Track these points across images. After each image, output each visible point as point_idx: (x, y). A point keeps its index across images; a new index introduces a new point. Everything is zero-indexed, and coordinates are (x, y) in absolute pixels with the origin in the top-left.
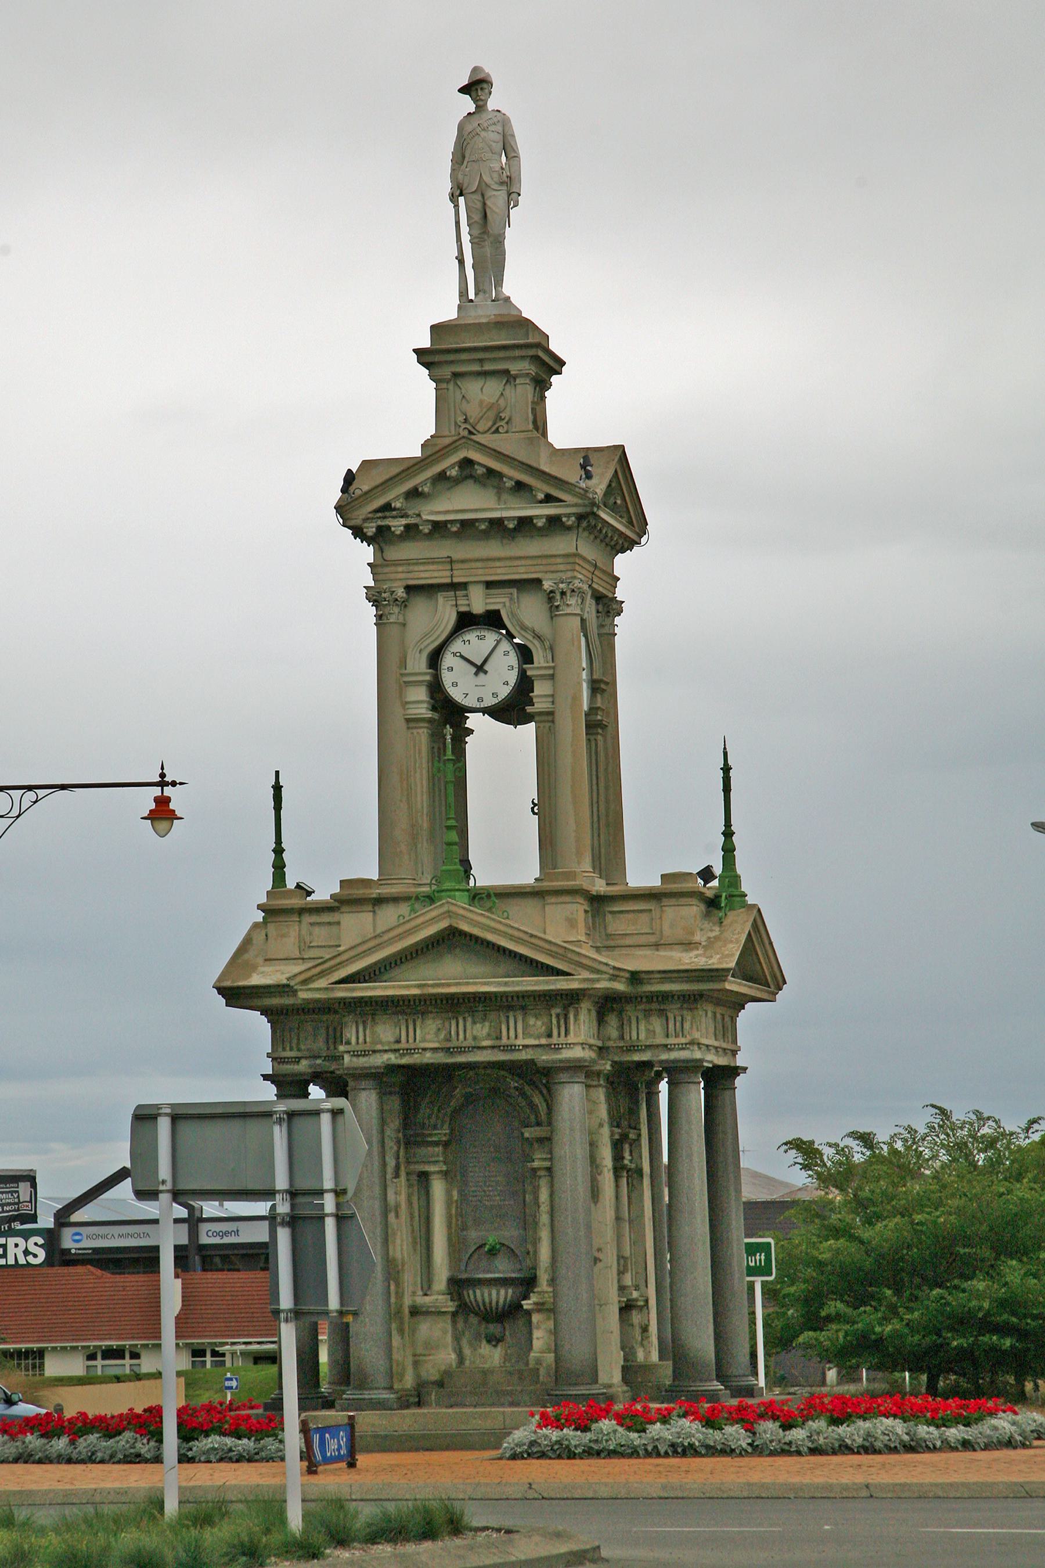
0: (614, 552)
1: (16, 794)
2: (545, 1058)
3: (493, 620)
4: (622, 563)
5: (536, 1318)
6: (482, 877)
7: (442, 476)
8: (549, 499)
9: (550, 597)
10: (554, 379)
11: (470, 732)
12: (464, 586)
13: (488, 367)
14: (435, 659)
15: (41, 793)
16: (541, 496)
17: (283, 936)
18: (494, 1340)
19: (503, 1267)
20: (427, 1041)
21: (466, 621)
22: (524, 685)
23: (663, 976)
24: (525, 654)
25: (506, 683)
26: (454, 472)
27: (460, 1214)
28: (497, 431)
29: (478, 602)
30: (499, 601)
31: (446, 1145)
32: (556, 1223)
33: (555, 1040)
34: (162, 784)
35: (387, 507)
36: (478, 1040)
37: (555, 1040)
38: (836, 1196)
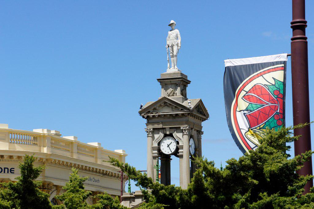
3: (171, 135)
4: (203, 124)
8: (182, 110)
10: (188, 85)
11: (172, 159)
16: (180, 109)
17: (126, 203)
21: (166, 136)
22: (177, 149)
24: (178, 143)
25: (174, 149)
28: (174, 96)
38: (307, 198)
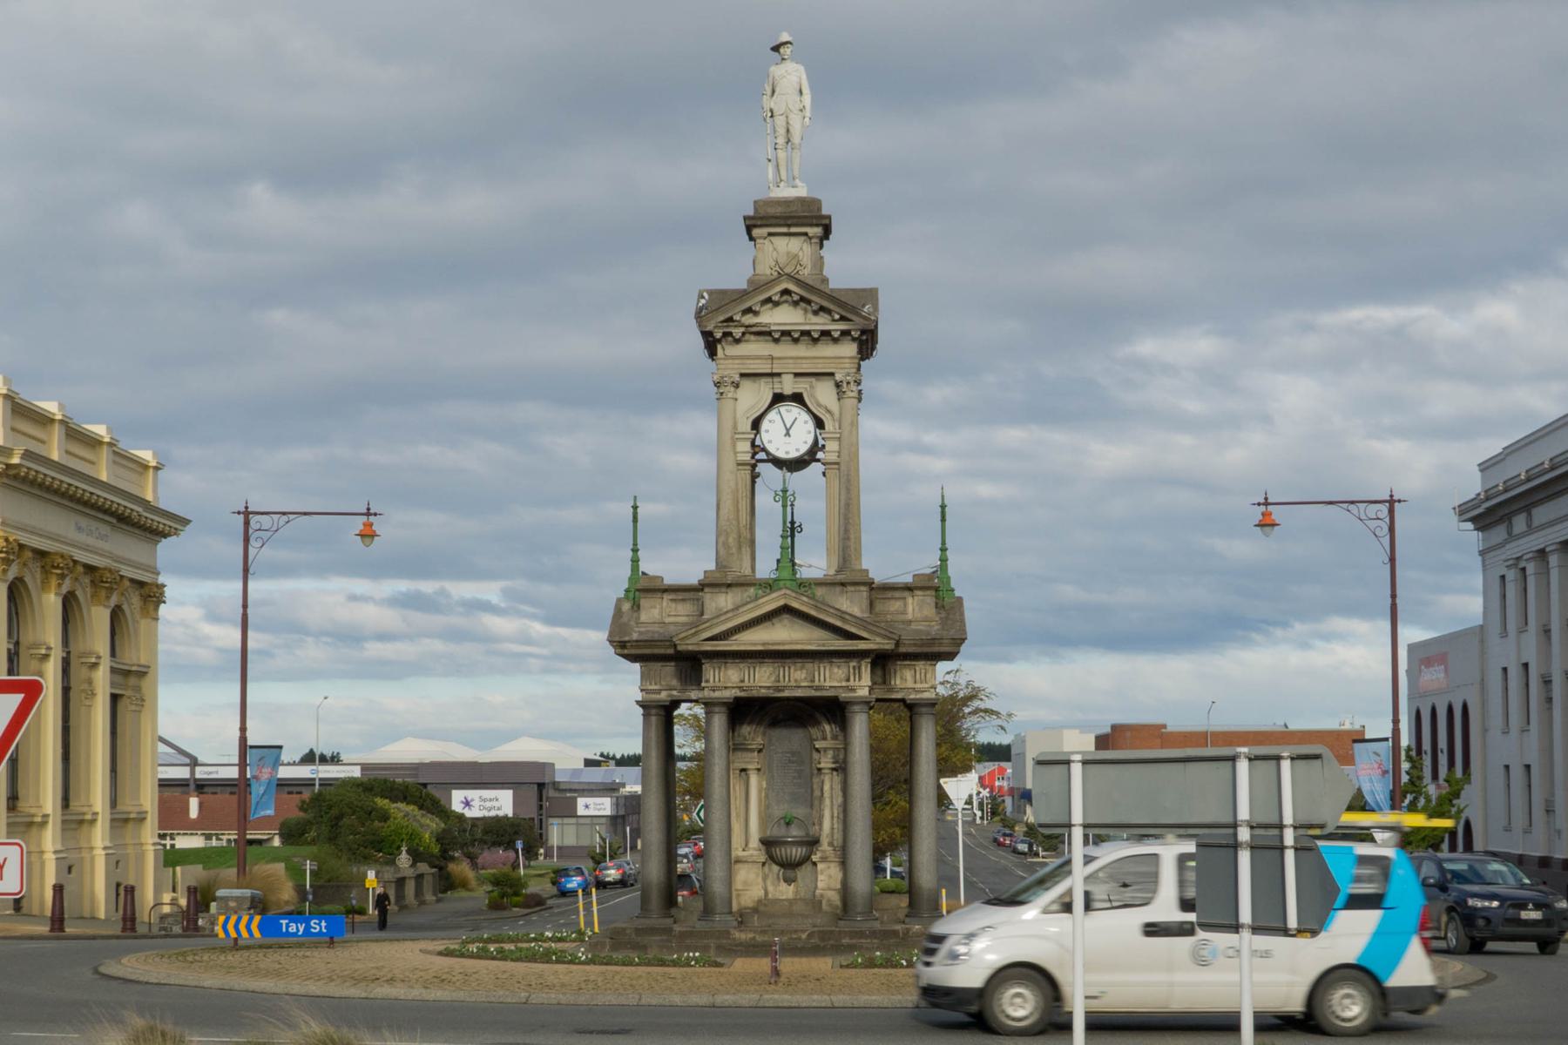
0: (152, 608)
1: (276, 517)
2: (844, 695)
3: (798, 398)
5: (820, 866)
6: (805, 573)
7: (769, 300)
8: (843, 318)
9: (838, 385)
12: (779, 375)
13: (793, 230)
14: (756, 425)
15: (1386, 541)
18: (789, 881)
19: (796, 832)
20: (762, 680)
21: (778, 399)
23: (936, 649)
26: (776, 298)
27: (767, 796)
29: (788, 386)
30: (801, 386)
31: (760, 751)
32: (659, 665)
33: (851, 683)
34: (1266, 504)
35: (730, 319)
36: (797, 681)
37: (851, 683)
